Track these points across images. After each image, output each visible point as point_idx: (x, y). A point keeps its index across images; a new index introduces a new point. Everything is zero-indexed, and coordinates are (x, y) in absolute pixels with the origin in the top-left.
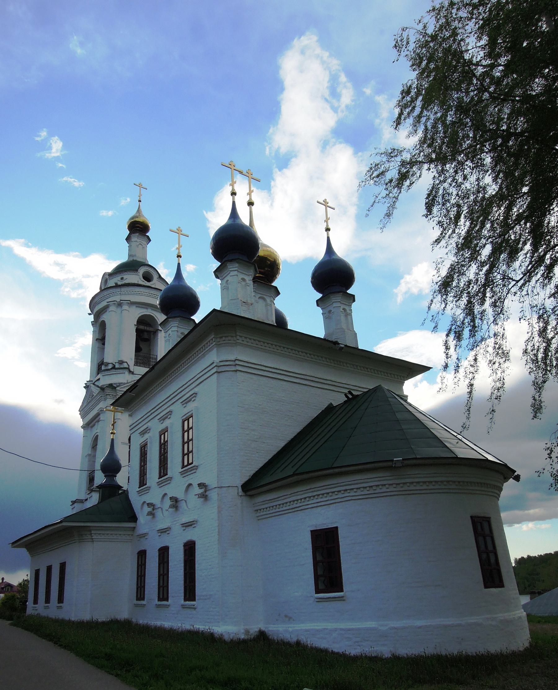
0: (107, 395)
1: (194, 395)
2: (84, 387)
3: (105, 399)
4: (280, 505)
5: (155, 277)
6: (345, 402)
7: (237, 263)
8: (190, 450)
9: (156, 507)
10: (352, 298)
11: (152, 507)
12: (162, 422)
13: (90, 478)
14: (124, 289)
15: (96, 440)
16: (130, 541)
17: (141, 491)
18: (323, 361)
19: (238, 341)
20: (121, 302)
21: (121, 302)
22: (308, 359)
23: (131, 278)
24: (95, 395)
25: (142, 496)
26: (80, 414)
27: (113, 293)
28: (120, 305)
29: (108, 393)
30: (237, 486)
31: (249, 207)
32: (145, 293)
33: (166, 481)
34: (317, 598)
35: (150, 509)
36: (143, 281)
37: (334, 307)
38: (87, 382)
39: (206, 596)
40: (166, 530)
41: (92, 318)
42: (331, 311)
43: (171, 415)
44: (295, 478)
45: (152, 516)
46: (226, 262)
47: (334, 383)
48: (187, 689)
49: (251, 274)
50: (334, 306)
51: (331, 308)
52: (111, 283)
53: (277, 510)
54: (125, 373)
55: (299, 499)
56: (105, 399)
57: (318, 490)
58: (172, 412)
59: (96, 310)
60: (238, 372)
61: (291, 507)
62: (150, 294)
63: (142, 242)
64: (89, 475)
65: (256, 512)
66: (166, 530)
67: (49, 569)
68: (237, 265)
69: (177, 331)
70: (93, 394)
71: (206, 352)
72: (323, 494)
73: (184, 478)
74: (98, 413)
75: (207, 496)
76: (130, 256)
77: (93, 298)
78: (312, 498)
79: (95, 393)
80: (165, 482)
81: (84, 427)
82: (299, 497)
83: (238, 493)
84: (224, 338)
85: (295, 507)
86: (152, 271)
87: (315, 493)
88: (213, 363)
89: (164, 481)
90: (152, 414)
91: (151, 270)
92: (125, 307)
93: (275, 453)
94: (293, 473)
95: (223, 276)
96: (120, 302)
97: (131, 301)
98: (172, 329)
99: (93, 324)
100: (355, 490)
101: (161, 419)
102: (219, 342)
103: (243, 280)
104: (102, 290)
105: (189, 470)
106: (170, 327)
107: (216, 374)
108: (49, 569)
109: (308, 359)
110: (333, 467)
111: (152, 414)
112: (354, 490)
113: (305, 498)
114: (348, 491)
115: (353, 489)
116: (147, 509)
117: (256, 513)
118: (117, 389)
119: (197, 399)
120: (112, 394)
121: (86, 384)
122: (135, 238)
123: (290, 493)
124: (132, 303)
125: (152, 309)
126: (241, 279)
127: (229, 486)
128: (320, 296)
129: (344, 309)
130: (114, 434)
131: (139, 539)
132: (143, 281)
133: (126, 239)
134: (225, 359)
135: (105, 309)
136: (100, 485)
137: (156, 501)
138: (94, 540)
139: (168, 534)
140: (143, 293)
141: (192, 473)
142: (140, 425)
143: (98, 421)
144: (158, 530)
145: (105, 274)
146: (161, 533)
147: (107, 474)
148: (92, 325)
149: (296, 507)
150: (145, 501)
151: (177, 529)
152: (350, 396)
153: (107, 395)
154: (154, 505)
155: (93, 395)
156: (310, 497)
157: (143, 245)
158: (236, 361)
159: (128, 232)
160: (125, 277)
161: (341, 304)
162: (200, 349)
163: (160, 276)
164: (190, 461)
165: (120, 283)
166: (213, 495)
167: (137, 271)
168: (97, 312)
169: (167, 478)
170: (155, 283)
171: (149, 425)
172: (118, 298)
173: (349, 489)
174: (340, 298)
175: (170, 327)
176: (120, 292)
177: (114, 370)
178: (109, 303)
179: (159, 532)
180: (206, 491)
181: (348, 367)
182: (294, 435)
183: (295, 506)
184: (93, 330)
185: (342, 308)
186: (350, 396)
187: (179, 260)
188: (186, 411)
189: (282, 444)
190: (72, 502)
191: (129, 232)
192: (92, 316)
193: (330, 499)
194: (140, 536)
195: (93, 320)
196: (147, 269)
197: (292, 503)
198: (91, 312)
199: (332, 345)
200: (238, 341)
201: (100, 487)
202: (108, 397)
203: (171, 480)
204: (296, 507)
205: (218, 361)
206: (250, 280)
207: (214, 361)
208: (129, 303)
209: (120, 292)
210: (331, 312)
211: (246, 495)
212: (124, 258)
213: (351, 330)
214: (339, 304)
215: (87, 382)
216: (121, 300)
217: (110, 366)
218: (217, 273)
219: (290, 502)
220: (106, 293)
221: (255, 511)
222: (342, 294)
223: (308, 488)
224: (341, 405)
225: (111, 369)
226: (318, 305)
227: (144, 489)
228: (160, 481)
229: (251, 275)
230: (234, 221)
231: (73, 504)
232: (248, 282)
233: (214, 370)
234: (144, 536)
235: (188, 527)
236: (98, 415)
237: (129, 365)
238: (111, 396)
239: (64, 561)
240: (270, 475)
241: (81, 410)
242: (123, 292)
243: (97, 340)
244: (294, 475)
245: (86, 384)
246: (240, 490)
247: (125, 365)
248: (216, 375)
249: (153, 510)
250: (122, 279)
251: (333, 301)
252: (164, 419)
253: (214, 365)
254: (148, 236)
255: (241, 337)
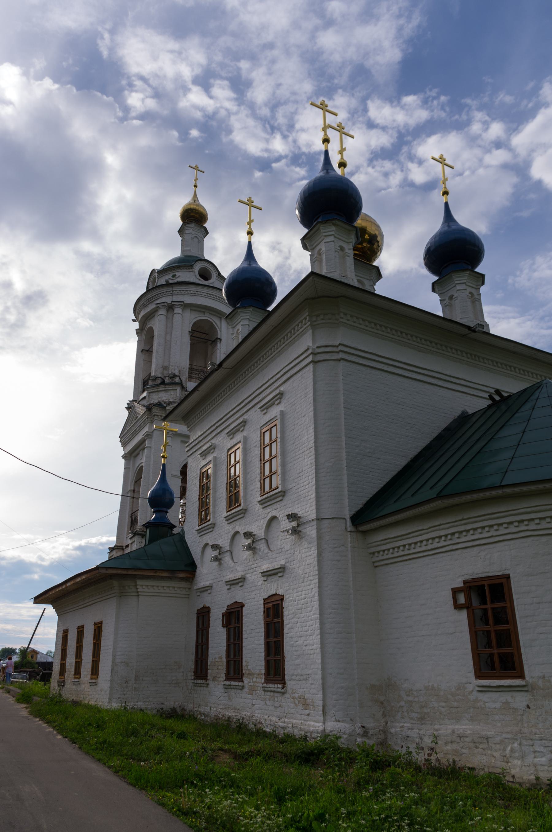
0: (154, 416)
1: (278, 396)
2: (126, 408)
3: (152, 421)
4: (410, 545)
5: (214, 275)
6: (489, 407)
7: (334, 225)
8: (273, 471)
9: (223, 550)
10: (482, 279)
11: (218, 550)
12: (231, 436)
13: (132, 520)
14: (177, 288)
15: (140, 470)
16: (187, 596)
17: (201, 530)
18: (453, 353)
19: (341, 320)
20: (173, 303)
21: (173, 303)
22: (433, 349)
23: (183, 276)
24: (139, 416)
25: (203, 536)
26: (120, 441)
27: (163, 293)
28: (170, 308)
29: (155, 414)
30: (344, 518)
31: (344, 158)
32: (202, 293)
33: (239, 515)
34: (479, 686)
35: (216, 553)
36: (199, 280)
37: (457, 290)
38: (129, 402)
39: (301, 675)
40: (237, 581)
41: (136, 325)
42: (453, 296)
43: (244, 426)
44: (439, 504)
45: (217, 563)
46: (319, 224)
47: (468, 384)
48: (519, 831)
49: (351, 240)
50: (458, 289)
51: (452, 292)
52: (162, 281)
53: (407, 552)
54: (176, 389)
55: (443, 536)
56: (152, 421)
57: (476, 522)
58: (245, 422)
59: (142, 313)
60: (341, 361)
61: (430, 547)
62: (208, 295)
63: (199, 234)
64: (130, 516)
65: (371, 556)
66: (237, 581)
67: (81, 631)
68: (334, 228)
69: (248, 325)
70: (138, 415)
71: (296, 337)
72: (483, 528)
73: (264, 509)
74: (143, 438)
75: (300, 531)
76: (183, 251)
77: (138, 300)
78: (464, 534)
79: (140, 414)
80: (236, 516)
81: (125, 456)
82: (443, 533)
83: (346, 528)
84: (322, 317)
85: (436, 547)
86: (210, 268)
87: (468, 527)
88: (308, 349)
89: (235, 514)
90: (217, 427)
91: (209, 267)
92: (178, 310)
93: (394, 473)
94: (437, 495)
95: (313, 244)
96: (171, 303)
97: (185, 302)
98: (241, 323)
99: (139, 332)
100: (537, 521)
101: (230, 433)
102: (315, 321)
103: (342, 249)
104: (148, 290)
105: (272, 498)
106: (239, 321)
107: (312, 364)
108: (81, 631)
109: (433, 349)
110: (502, 484)
111: (217, 427)
112: (535, 520)
113: (453, 534)
114: (526, 523)
115: (533, 520)
116: (211, 553)
117: (372, 557)
118: (167, 408)
119: (284, 401)
120: (160, 414)
121: (128, 404)
122: (192, 229)
123: (427, 527)
124: (186, 306)
125: (210, 314)
126: (339, 246)
127: (333, 518)
128: (436, 278)
129: (470, 293)
130: (166, 458)
131: (198, 594)
132: (199, 280)
133: (178, 232)
134: (324, 343)
135: (153, 313)
136: (147, 523)
137: (224, 542)
138: (140, 593)
139: (241, 586)
140: (200, 293)
141: (277, 502)
142: (201, 444)
143: (144, 449)
144: (226, 582)
145: (153, 271)
146: (231, 585)
147: (156, 509)
148: (137, 333)
149: (438, 548)
150: (208, 542)
151: (255, 578)
152: (497, 398)
153: (154, 416)
154: (221, 547)
155: (137, 417)
156: (461, 532)
157: (199, 238)
158: (340, 346)
159: (181, 223)
160: (178, 274)
161: (467, 287)
162: (295, 327)
163: (219, 274)
164: (274, 486)
165: (171, 281)
166: (311, 531)
167: (192, 266)
168: (143, 316)
169: (239, 511)
170: (213, 281)
171: (213, 442)
172: (168, 300)
173: (526, 520)
174: (466, 278)
175: (239, 321)
176: (171, 292)
177: (163, 386)
178: (158, 306)
179: (228, 585)
180: (298, 525)
181: (485, 363)
182: (418, 451)
183: (435, 545)
184: (137, 340)
185: (468, 291)
186: (497, 398)
187: (250, 238)
188: (267, 418)
189: (403, 462)
190: (109, 548)
191: (182, 223)
192: (137, 323)
193: (494, 535)
194: (200, 590)
195: (138, 328)
196: (204, 264)
197: (430, 541)
198: (135, 319)
199: (466, 331)
200: (341, 320)
201: (148, 525)
202: (156, 418)
203: (245, 513)
204: (438, 548)
205: (315, 347)
206: (351, 249)
207: (308, 346)
208: (182, 305)
209: (171, 292)
210: (453, 297)
211: (358, 531)
212: (176, 253)
213: (481, 320)
214: (464, 286)
215: (129, 402)
216: (172, 301)
217: (159, 381)
218: (305, 241)
219: (427, 540)
220: (154, 293)
221: (370, 554)
222: (468, 272)
223: (460, 518)
224: (485, 410)
225: (160, 384)
226: (434, 290)
227: (206, 526)
228: (229, 515)
229: (351, 242)
230: (327, 172)
231: (112, 551)
232: (347, 251)
233: (310, 359)
234: (207, 589)
235: (271, 577)
236: (143, 441)
237: (181, 380)
238: (159, 417)
239: (100, 621)
240: (395, 502)
241: (121, 436)
242: (174, 292)
243: (144, 351)
244: (439, 496)
245: (128, 404)
246: (349, 523)
247: (177, 380)
248: (311, 366)
249: (220, 554)
250: (174, 276)
251: (456, 282)
252: (234, 434)
253: (310, 351)
254: (205, 227)
255: (345, 314)
